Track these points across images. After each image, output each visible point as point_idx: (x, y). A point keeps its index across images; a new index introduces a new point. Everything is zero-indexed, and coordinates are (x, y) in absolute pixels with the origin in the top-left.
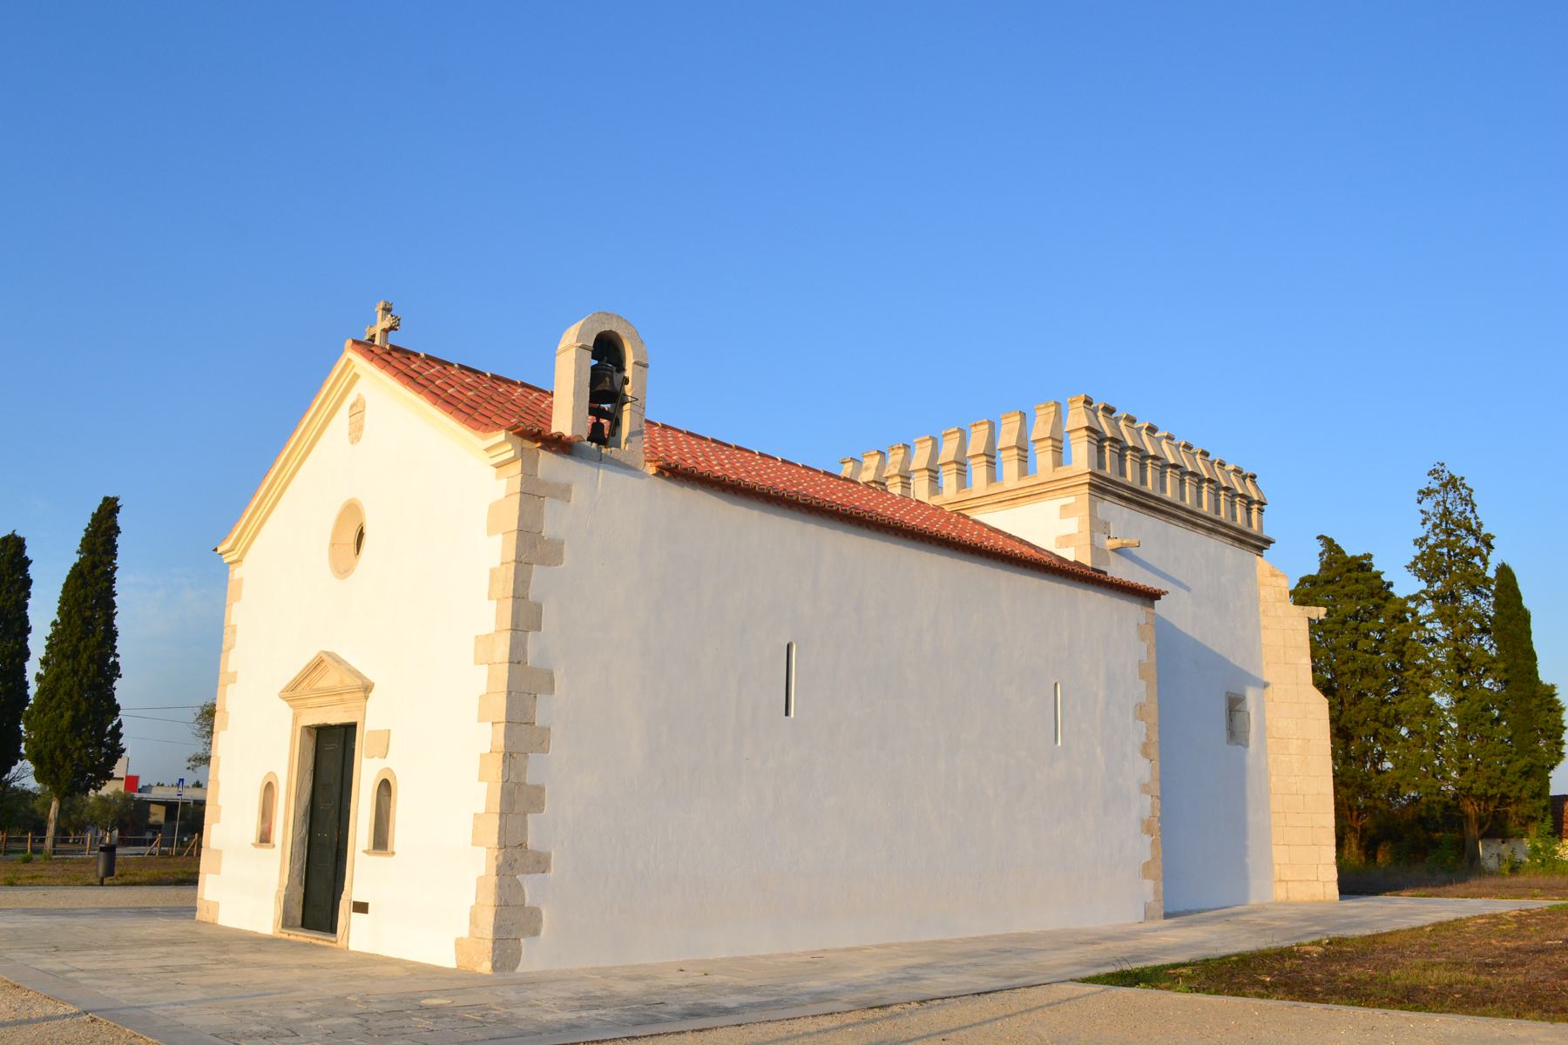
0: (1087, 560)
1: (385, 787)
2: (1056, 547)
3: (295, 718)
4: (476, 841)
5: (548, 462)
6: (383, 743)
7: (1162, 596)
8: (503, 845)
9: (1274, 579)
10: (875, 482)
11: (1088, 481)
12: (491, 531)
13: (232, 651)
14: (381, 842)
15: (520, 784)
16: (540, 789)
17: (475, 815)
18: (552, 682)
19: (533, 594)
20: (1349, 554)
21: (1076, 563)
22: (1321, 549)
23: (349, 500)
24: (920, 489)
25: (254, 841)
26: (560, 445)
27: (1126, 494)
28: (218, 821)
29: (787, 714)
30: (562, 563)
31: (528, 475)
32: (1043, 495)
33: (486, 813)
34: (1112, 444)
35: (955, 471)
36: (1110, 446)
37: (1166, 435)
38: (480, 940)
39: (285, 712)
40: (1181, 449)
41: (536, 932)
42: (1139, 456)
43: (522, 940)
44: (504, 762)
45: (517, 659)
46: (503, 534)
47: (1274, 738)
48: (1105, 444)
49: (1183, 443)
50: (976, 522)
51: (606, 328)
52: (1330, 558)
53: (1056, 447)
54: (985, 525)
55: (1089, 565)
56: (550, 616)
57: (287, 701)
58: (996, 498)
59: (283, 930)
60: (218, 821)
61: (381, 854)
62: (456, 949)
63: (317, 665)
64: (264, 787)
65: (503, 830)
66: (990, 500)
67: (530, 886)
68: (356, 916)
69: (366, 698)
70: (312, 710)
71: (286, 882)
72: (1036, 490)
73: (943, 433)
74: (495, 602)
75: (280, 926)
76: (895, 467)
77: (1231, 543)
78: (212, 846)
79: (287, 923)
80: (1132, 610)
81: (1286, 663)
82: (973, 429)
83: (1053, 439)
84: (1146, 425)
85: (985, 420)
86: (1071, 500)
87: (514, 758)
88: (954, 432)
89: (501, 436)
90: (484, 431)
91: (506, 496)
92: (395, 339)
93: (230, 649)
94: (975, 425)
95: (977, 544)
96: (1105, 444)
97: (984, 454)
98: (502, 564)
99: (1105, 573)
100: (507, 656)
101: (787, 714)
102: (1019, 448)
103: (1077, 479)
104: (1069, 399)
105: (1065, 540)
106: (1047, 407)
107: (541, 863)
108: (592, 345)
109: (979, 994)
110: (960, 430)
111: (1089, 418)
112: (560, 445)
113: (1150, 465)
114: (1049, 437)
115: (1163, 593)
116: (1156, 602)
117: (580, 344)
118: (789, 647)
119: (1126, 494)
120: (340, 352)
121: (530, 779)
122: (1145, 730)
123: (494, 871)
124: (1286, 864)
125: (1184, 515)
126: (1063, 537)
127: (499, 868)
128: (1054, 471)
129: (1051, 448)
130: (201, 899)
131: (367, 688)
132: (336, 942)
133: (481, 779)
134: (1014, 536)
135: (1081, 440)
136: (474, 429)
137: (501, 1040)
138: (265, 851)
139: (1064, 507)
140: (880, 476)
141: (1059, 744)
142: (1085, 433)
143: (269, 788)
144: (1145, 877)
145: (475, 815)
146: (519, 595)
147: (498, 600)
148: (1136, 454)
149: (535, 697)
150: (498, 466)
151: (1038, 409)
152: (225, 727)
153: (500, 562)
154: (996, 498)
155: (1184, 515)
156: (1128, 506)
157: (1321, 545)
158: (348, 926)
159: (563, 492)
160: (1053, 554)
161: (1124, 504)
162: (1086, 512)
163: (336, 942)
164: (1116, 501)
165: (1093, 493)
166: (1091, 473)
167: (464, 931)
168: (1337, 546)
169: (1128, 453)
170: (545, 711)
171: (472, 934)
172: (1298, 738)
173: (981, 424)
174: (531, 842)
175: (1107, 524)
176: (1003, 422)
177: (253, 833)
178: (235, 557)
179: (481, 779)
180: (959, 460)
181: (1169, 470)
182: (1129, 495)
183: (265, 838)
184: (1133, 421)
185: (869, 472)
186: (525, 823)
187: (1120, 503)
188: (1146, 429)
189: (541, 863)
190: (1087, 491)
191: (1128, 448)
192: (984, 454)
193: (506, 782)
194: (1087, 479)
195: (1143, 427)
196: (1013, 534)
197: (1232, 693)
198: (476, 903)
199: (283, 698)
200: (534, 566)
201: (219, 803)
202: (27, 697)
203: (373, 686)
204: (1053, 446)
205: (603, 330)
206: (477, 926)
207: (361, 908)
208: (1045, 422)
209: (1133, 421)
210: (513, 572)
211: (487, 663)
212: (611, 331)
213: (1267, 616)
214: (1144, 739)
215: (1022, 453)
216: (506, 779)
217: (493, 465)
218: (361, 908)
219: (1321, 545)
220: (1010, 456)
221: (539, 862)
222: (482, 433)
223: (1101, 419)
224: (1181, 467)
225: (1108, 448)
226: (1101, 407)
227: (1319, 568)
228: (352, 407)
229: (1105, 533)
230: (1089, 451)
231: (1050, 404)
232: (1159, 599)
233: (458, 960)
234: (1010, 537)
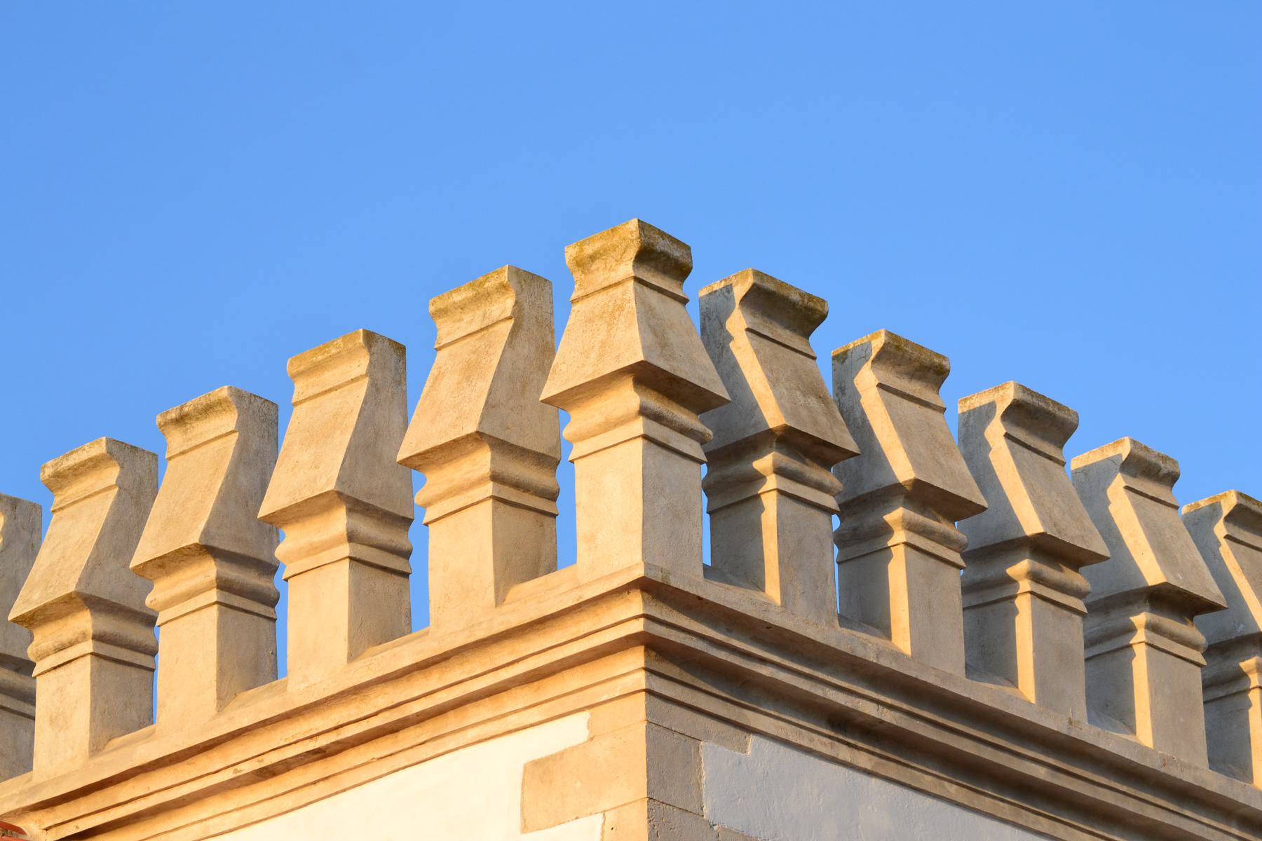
11: (638, 626)
32: (451, 721)
34: (794, 465)
35: (88, 646)
36: (780, 471)
37: (1125, 450)
40: (1220, 530)
42: (1201, 638)
48: (1012, 571)
49: (1229, 503)
53: (517, 485)
73: (49, 471)
82: (176, 440)
83: (501, 446)
84: (1007, 396)
85: (223, 392)
86: (573, 730)
88: (94, 464)
94: (181, 420)
96: (1012, 571)
97: (206, 549)
102: (357, 507)
103: (585, 623)
104: (570, 252)
106: (481, 298)
110: (121, 451)
113: (1025, 585)
114: (479, 437)
119: (870, 709)
129: (489, 488)
142: (628, 398)
151: (443, 312)
154: (244, 756)
156: (892, 770)
161: (864, 760)
164: (820, 744)
165: (658, 667)
166: (646, 586)
169: (896, 516)
173: (208, 410)
176: (301, 388)
180: (104, 589)
181: (1140, 619)
182: (889, 717)
184: (934, 373)
187: (844, 753)
188: (1006, 416)
190: (640, 680)
191: (892, 493)
192: (206, 549)
195: (992, 406)
204: (495, 478)
208: (469, 371)
209: (934, 373)
223: (1001, 457)
224: (1211, 607)
225: (772, 482)
226: (740, 291)
230: (652, 488)
231: (490, 284)
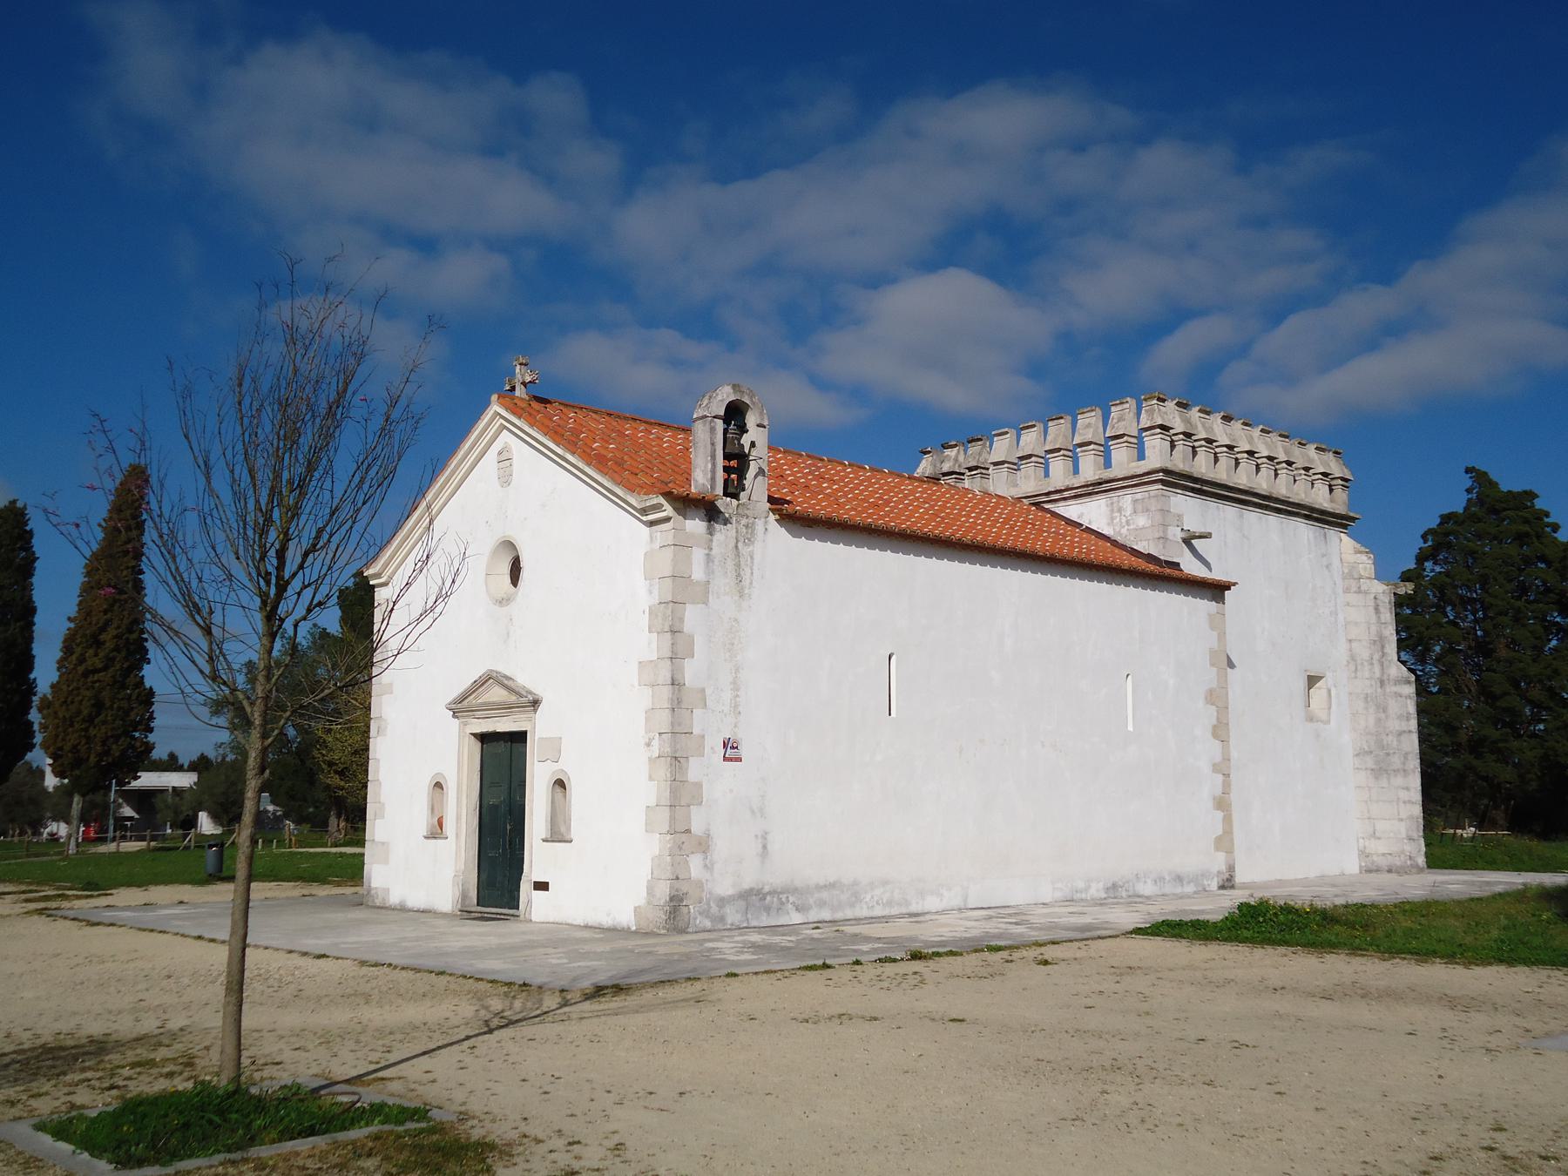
4: (649, 827)
6: (554, 749)
7: (1232, 587)
8: (672, 832)
14: (557, 835)
20: (1504, 487)
22: (1469, 483)
29: (890, 715)
63: (488, 679)
78: (1418, 806)
87: (679, 762)
101: (890, 715)
104: (1143, 397)
115: (1234, 584)
120: (487, 404)
122: (1215, 714)
131: (535, 703)
137: (786, 928)
144: (1217, 849)
147: (658, 633)
158: (529, 902)
177: (422, 826)
183: (437, 831)
202: (31, 687)
206: (654, 896)
207: (542, 886)
216: (673, 779)
218: (542, 886)
228: (500, 453)
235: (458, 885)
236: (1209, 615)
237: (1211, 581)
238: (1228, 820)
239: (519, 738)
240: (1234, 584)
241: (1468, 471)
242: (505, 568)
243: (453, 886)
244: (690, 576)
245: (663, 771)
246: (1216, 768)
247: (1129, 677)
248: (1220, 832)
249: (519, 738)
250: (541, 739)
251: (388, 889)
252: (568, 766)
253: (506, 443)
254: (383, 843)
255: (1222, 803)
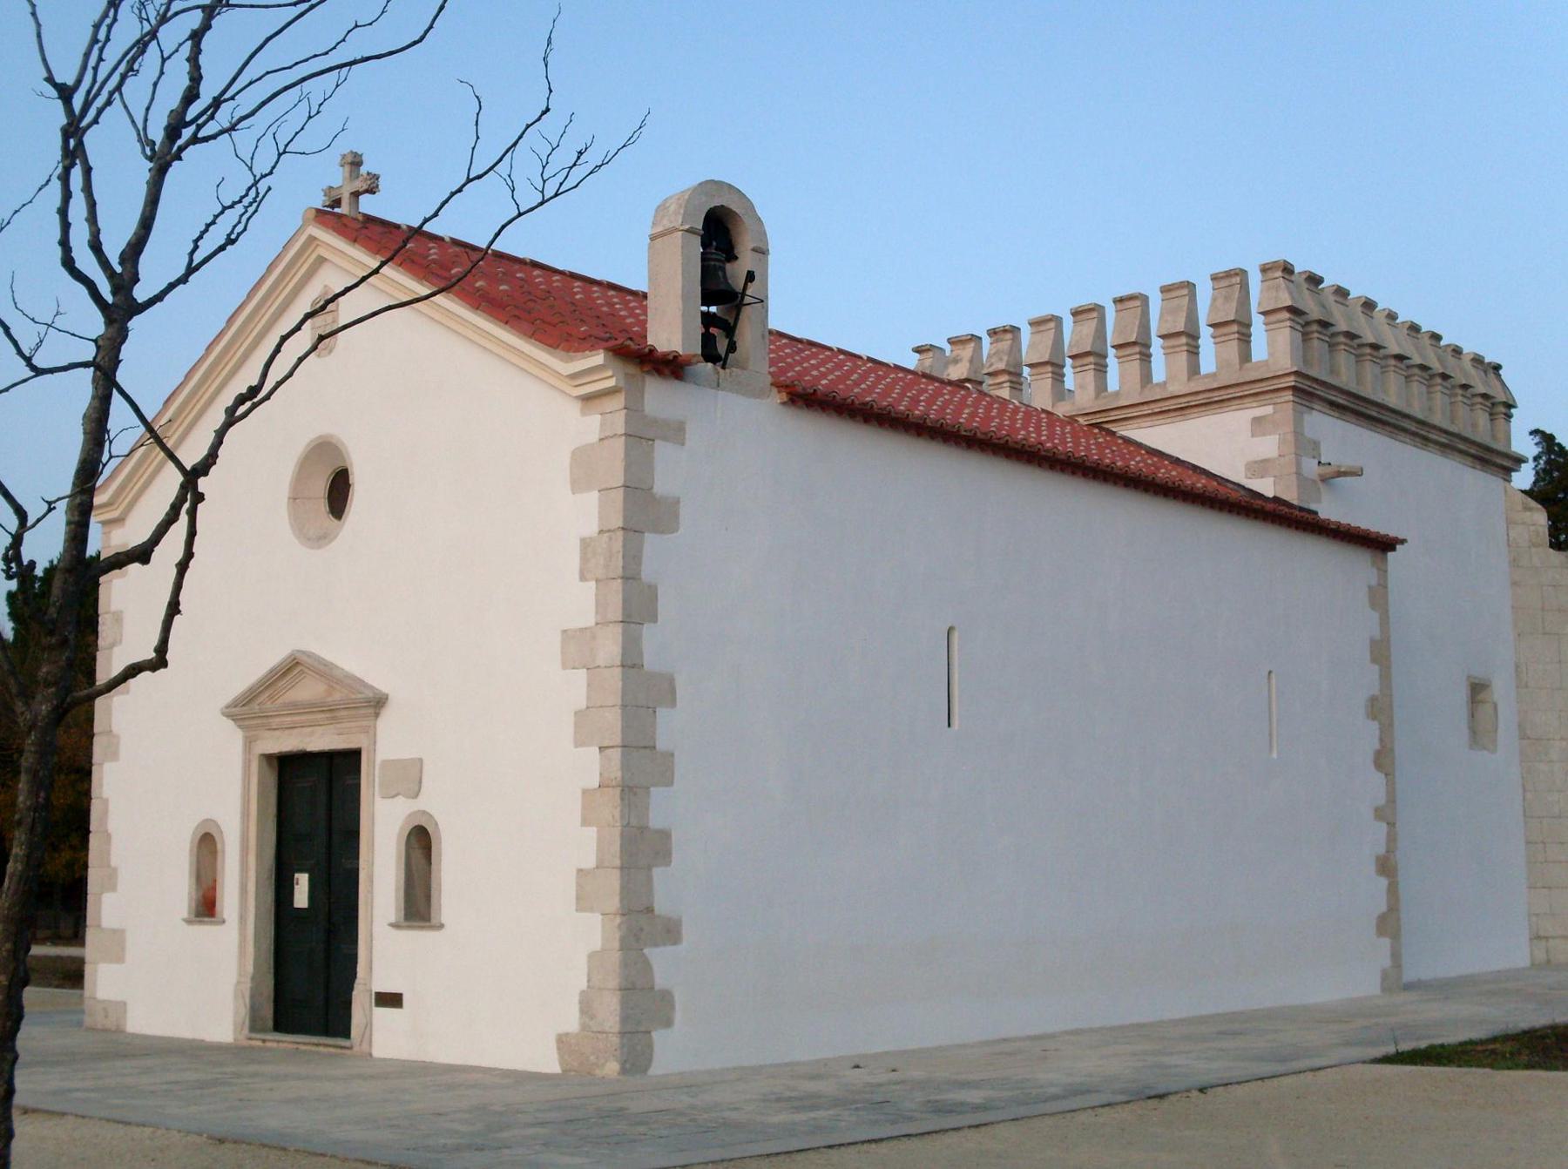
0: (1291, 496)
1: (421, 841)
2: (1247, 477)
3: (249, 743)
4: (583, 902)
5: (660, 396)
6: (410, 777)
7: (1398, 547)
8: (626, 912)
9: (1528, 513)
10: (968, 380)
11: (1293, 384)
12: (577, 485)
13: (116, 649)
15: (643, 829)
16: (665, 835)
17: (580, 871)
18: (673, 691)
19: (647, 572)
21: (1276, 499)
23: (320, 437)
24: (1039, 394)
25: (185, 915)
26: (670, 367)
27: (1341, 400)
28: (113, 888)
30: (677, 531)
31: (633, 409)
33: (597, 867)
38: (600, 1036)
39: (233, 737)
41: (668, 1023)
43: (654, 1034)
44: (622, 799)
45: (631, 663)
46: (599, 491)
47: (1529, 738)
50: (1128, 441)
51: (716, 203)
52: (1548, 462)
54: (1140, 445)
55: (1295, 502)
56: (666, 605)
57: (233, 720)
58: (1156, 408)
59: (254, 1035)
60: (113, 888)
61: (422, 928)
62: (559, 1049)
63: (292, 667)
64: (199, 837)
65: (626, 890)
66: (1146, 410)
67: (663, 963)
68: (383, 1014)
69: (377, 715)
70: (277, 733)
71: (250, 969)
72: (1216, 396)
74: (593, 584)
75: (246, 1031)
76: (1001, 359)
77: (1471, 465)
79: (255, 1026)
80: (1358, 562)
81: (1545, 634)
86: (1269, 410)
89: (598, 358)
90: (568, 351)
91: (601, 440)
92: (368, 205)
93: (112, 645)
95: (1174, 483)
98: (601, 532)
99: (1316, 513)
100: (619, 658)
105: (1260, 467)
107: (671, 932)
108: (700, 227)
109: (1262, 1079)
111: (1291, 293)
112: (670, 367)
115: (1403, 542)
116: (1390, 555)
117: (687, 227)
118: (950, 631)
119: (1341, 401)
121: (656, 821)
123: (617, 945)
124: (1545, 914)
125: (1413, 427)
126: (1256, 462)
127: (623, 940)
128: (1241, 369)
130: (90, 998)
132: (350, 1048)
133: (585, 822)
134: (1184, 462)
135: (1282, 324)
136: (550, 346)
138: (205, 931)
139: (1257, 421)
140: (975, 372)
141: (1275, 755)
143: (207, 844)
145: (580, 871)
146: (630, 576)
147: (597, 581)
148: (1297, 319)
149: (655, 712)
150: (587, 399)
152: (114, 755)
153: (597, 531)
154: (1156, 408)
155: (1413, 427)
157: (1536, 444)
158: (369, 1025)
159: (676, 432)
160: (1243, 488)
162: (1289, 428)
163: (350, 1048)
167: (571, 1022)
168: (1559, 445)
170: (670, 727)
171: (584, 1027)
172: (1562, 739)
174: (661, 906)
175: (1316, 445)
178: (115, 514)
179: (585, 822)
183: (206, 907)
185: (959, 365)
186: (650, 879)
187: (1333, 413)
188: (1408, 329)
189: (671, 932)
193: (626, 826)
194: (1185, 348)
196: (1181, 458)
197: (1475, 678)
198: (589, 987)
199: (228, 716)
200: (646, 534)
201: (113, 864)
203: (387, 699)
205: (712, 206)
207: (391, 1000)
210: (621, 544)
211: (584, 667)
212: (722, 206)
213: (1518, 566)
214: (1377, 746)
215: (1191, 341)
216: (625, 823)
217: (577, 397)
218: (391, 1000)
219: (1536, 444)
220: (1174, 347)
221: (669, 931)
222: (562, 353)
227: (1533, 479)
229: (1314, 457)
230: (1292, 342)
232: (1393, 549)
233: (562, 1061)
234: (1177, 462)
235: (243, 997)
236: (1370, 587)
237: (1374, 536)
238: (1393, 891)
239: (351, 758)
240: (1403, 542)
241: (1535, 432)
242: (321, 487)
243: (236, 997)
244: (652, 488)
245: (610, 808)
246: (1379, 814)
247: (1273, 675)
248: (1383, 908)
249: (351, 758)
250: (385, 763)
251: (125, 1004)
252: (435, 803)
253: (326, 286)
254: (114, 931)
255: (1386, 866)
